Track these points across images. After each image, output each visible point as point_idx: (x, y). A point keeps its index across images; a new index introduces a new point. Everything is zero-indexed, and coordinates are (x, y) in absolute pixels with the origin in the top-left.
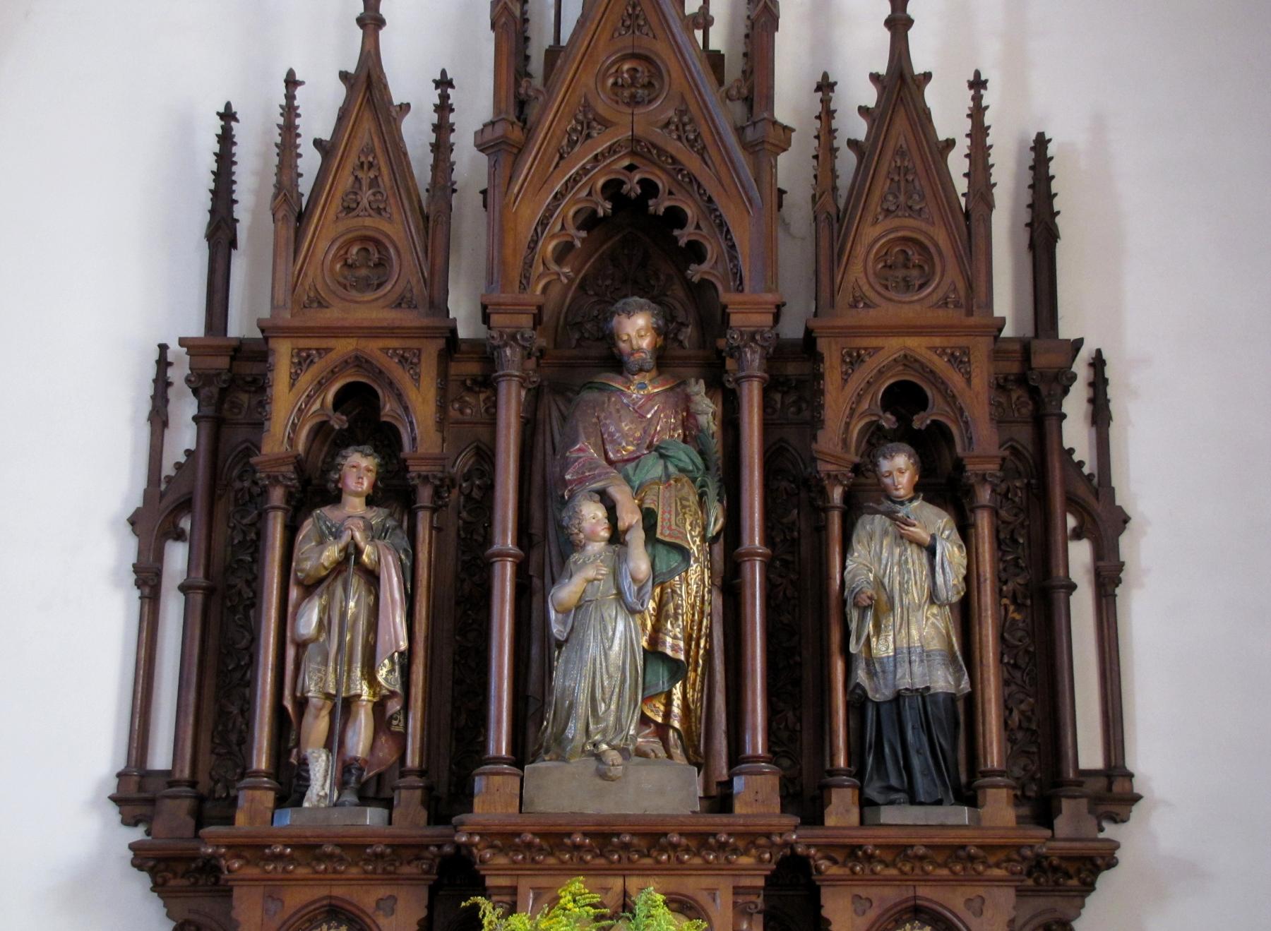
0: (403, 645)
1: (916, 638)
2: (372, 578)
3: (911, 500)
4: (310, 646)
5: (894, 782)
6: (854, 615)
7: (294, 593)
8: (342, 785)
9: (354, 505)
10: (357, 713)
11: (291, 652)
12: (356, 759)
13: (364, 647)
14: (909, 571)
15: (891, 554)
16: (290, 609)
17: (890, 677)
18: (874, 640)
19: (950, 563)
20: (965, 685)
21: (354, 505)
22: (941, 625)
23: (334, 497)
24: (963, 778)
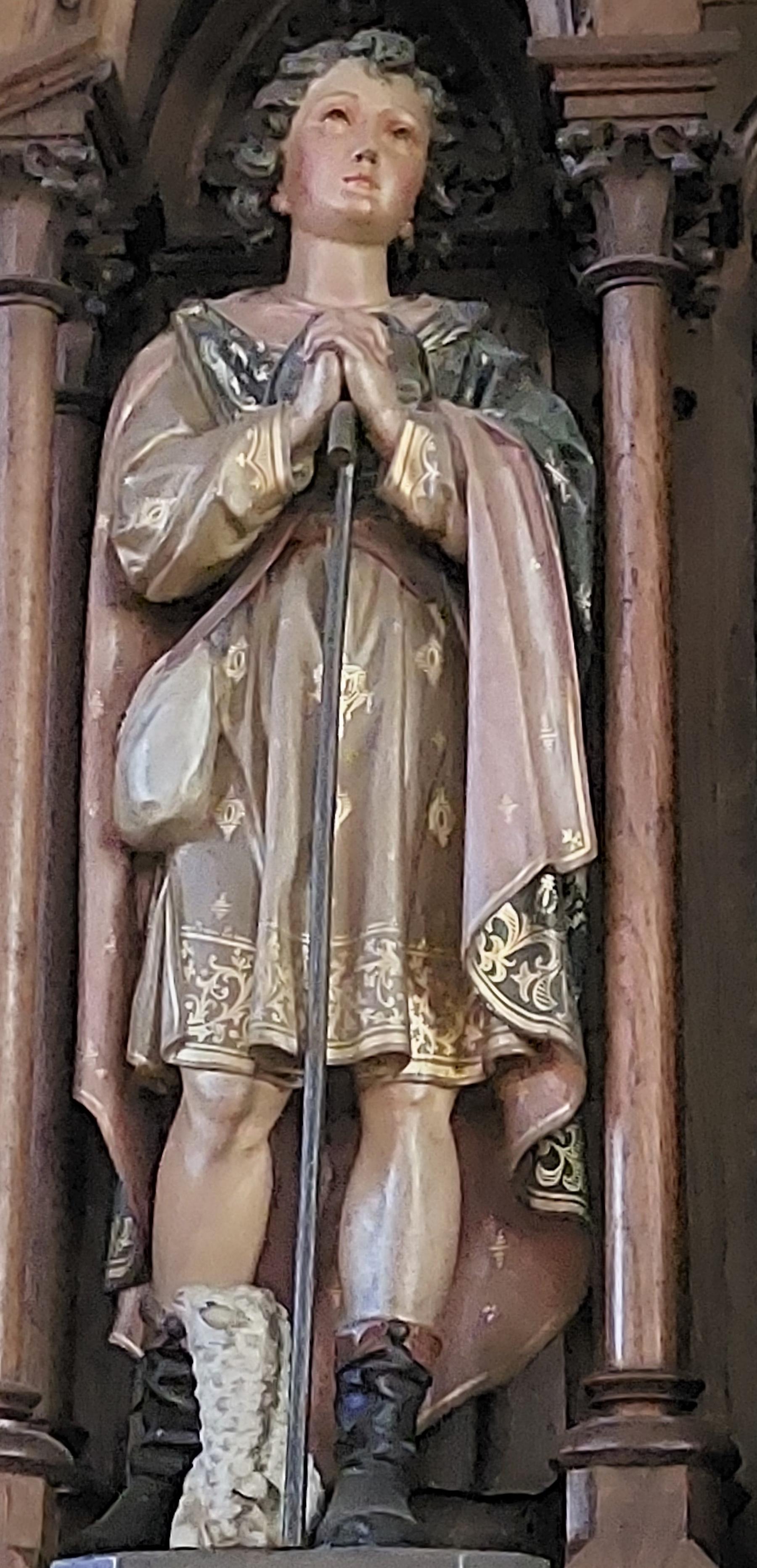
0: (578, 847)
2: (436, 566)
4: (183, 856)
7: (108, 639)
8: (333, 1444)
9: (337, 281)
10: (392, 1129)
11: (102, 884)
12: (394, 1332)
13: (411, 862)
16: (94, 705)
21: (337, 281)
23: (265, 263)
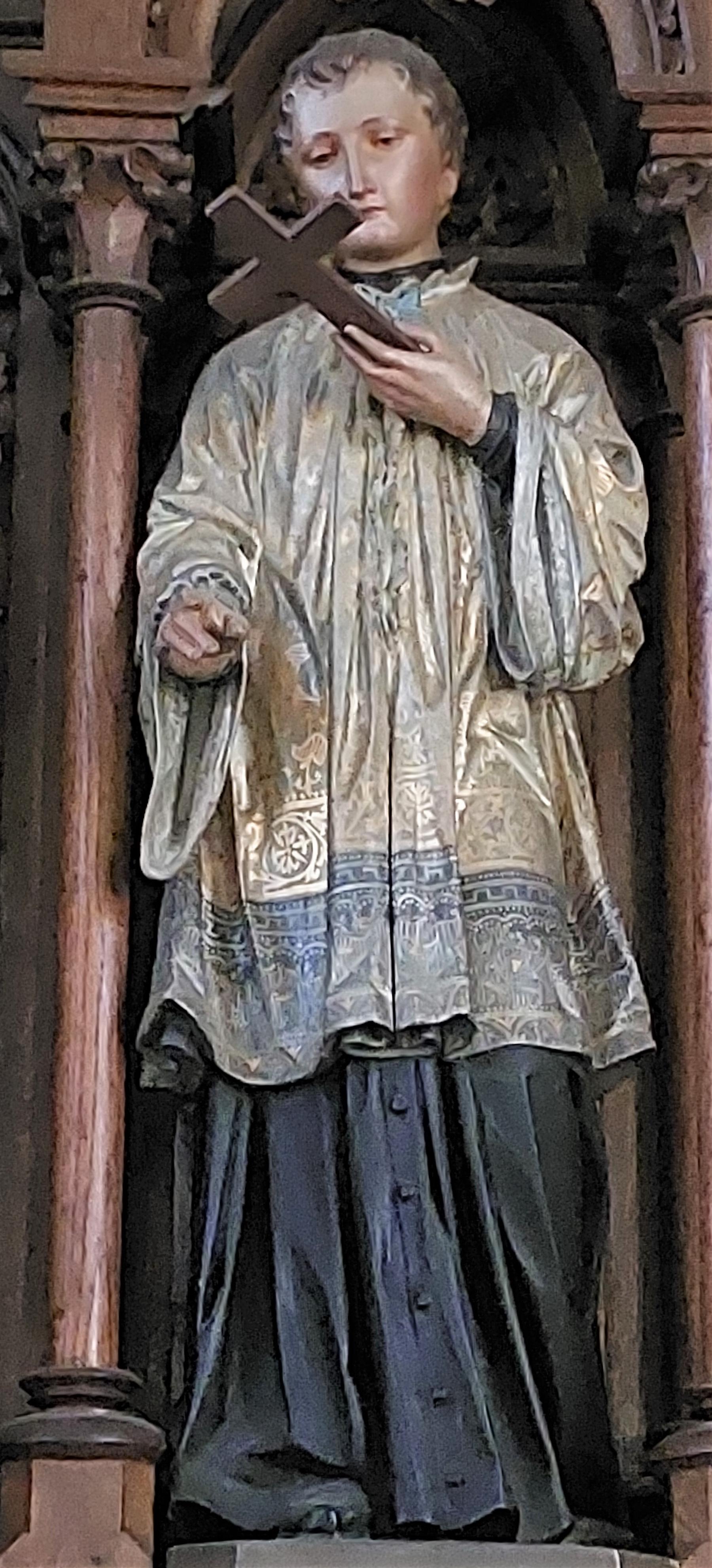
1: (401, 646)
3: (423, 271)
5: (311, 1432)
6: (165, 724)
14: (398, 544)
15: (332, 475)
17: (311, 982)
18: (250, 833)
19: (573, 517)
20: (631, 1025)
22: (534, 775)
24: (629, 1422)
